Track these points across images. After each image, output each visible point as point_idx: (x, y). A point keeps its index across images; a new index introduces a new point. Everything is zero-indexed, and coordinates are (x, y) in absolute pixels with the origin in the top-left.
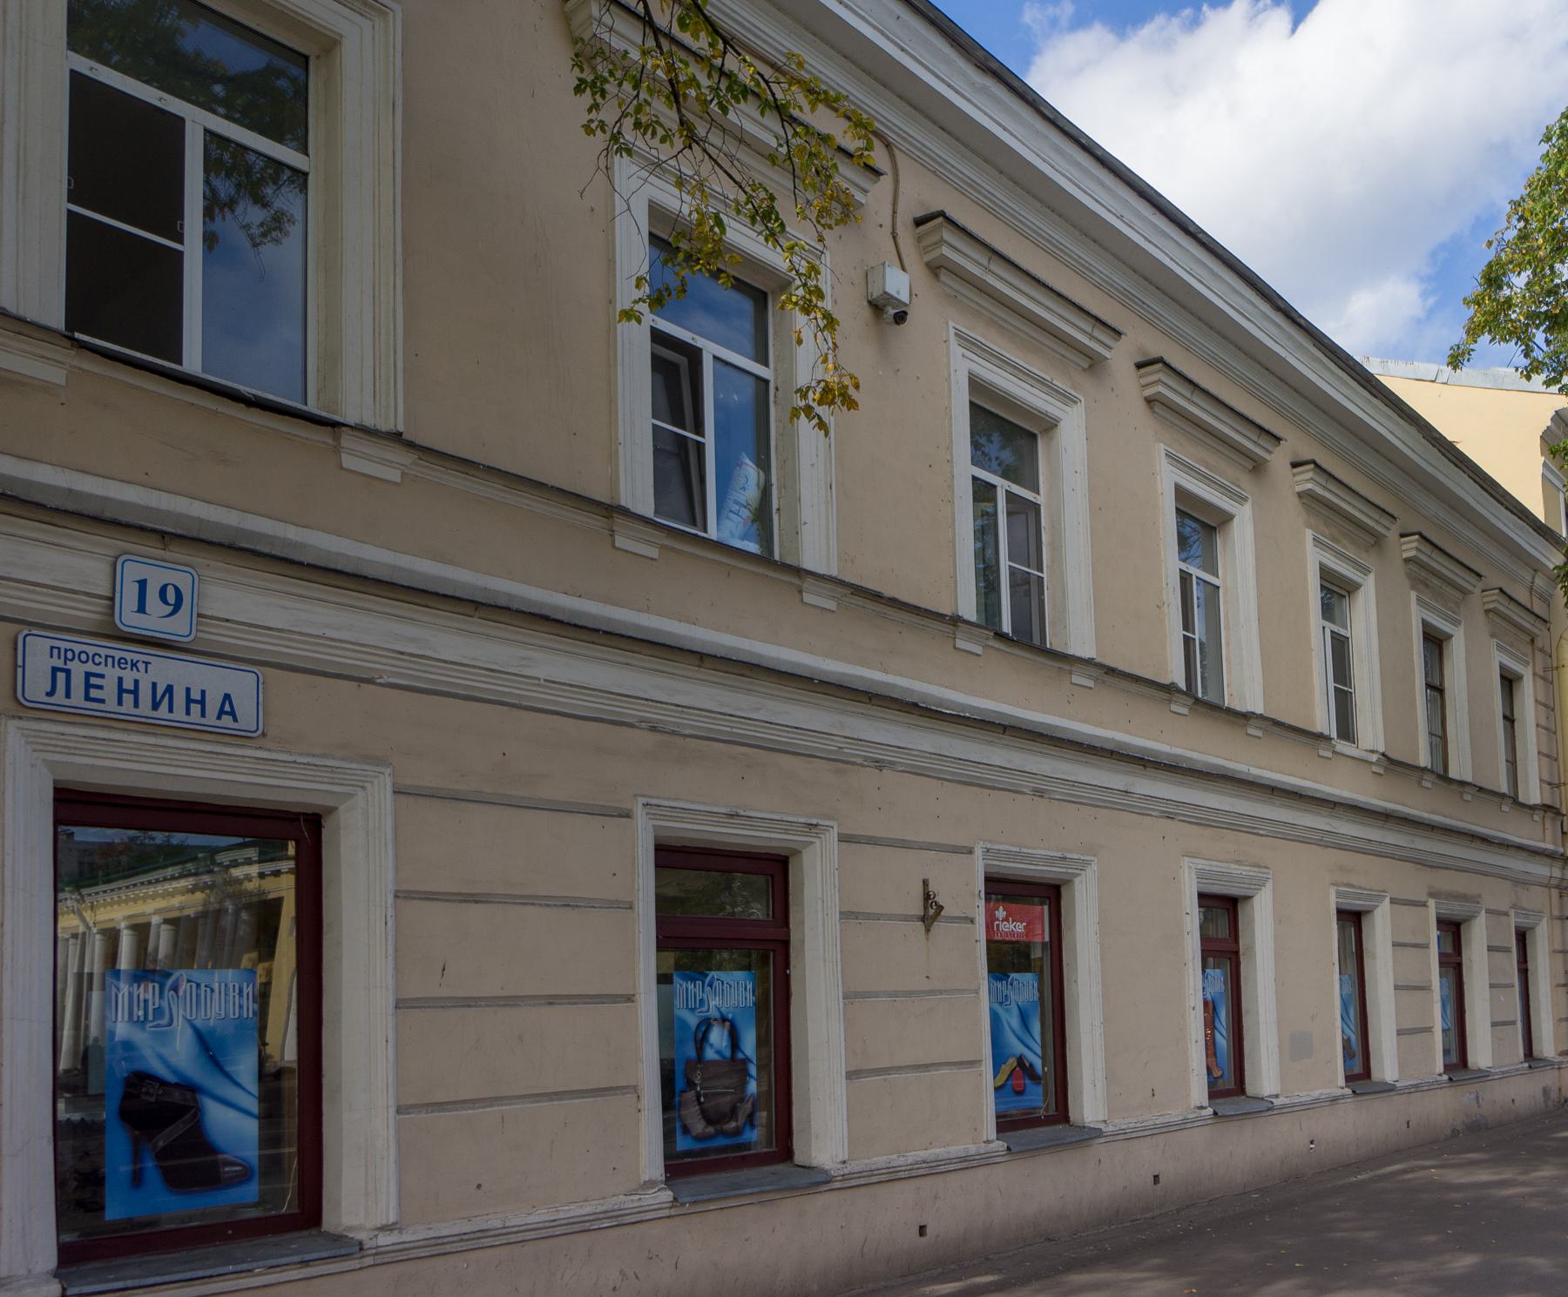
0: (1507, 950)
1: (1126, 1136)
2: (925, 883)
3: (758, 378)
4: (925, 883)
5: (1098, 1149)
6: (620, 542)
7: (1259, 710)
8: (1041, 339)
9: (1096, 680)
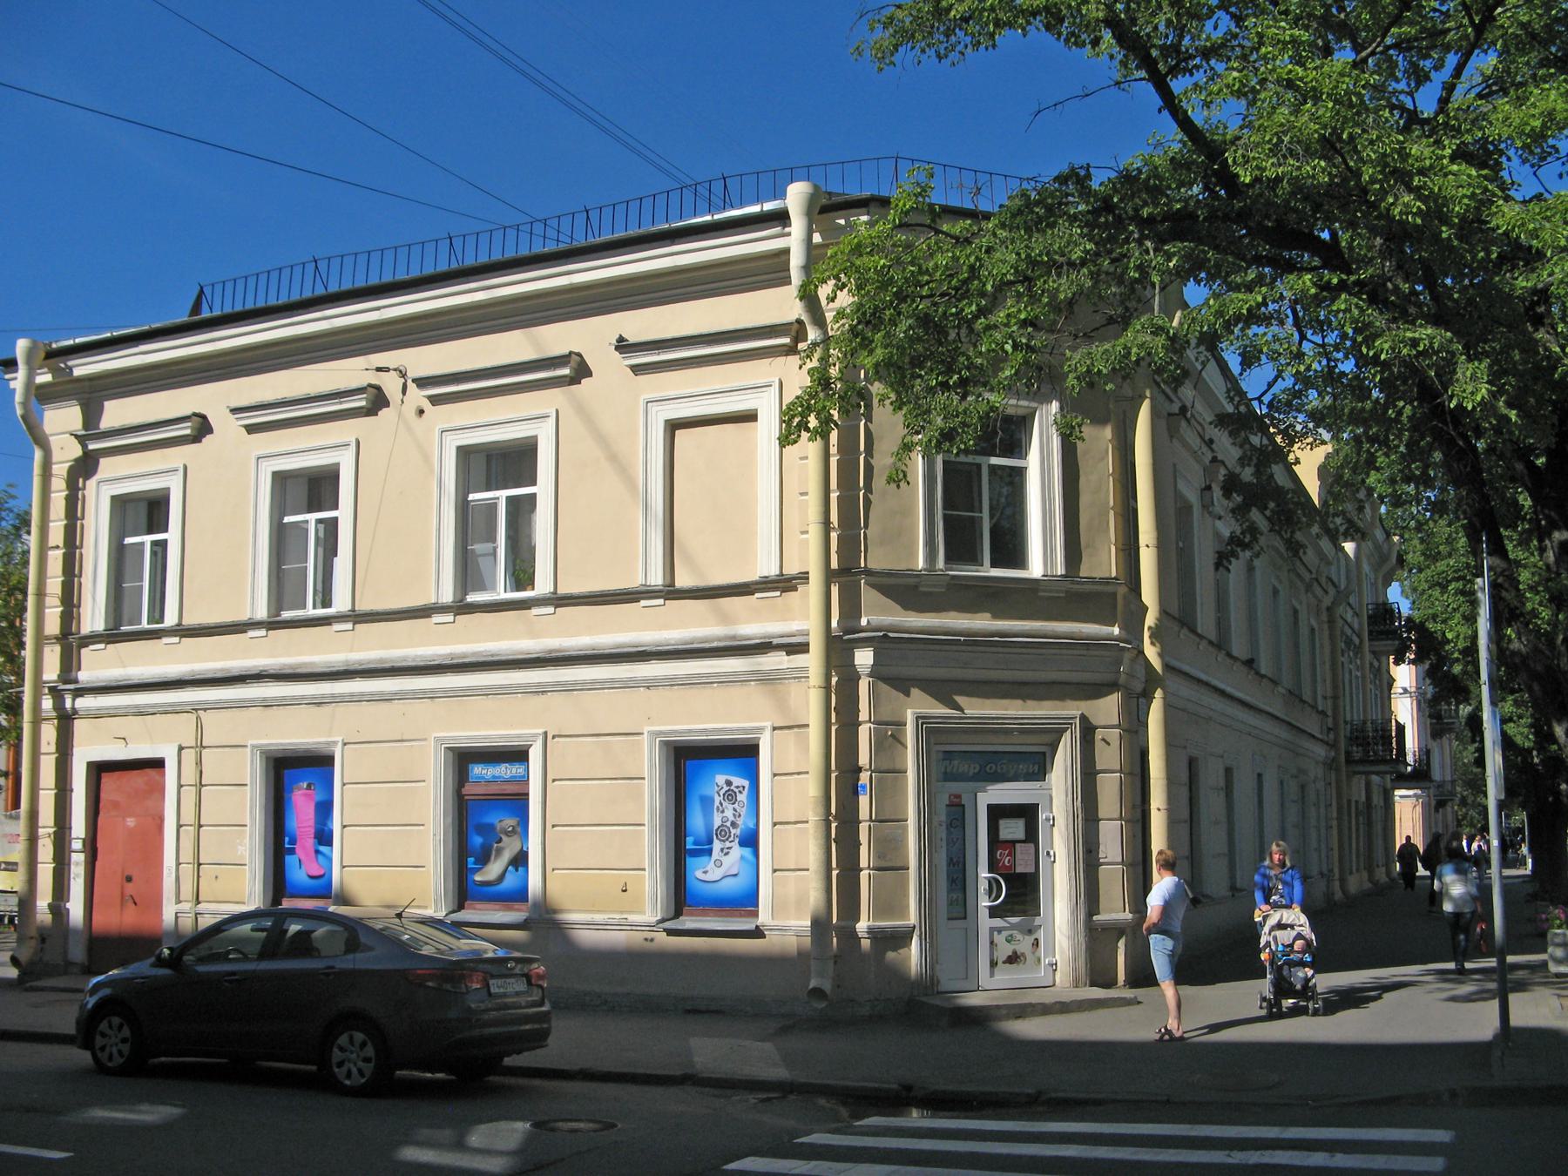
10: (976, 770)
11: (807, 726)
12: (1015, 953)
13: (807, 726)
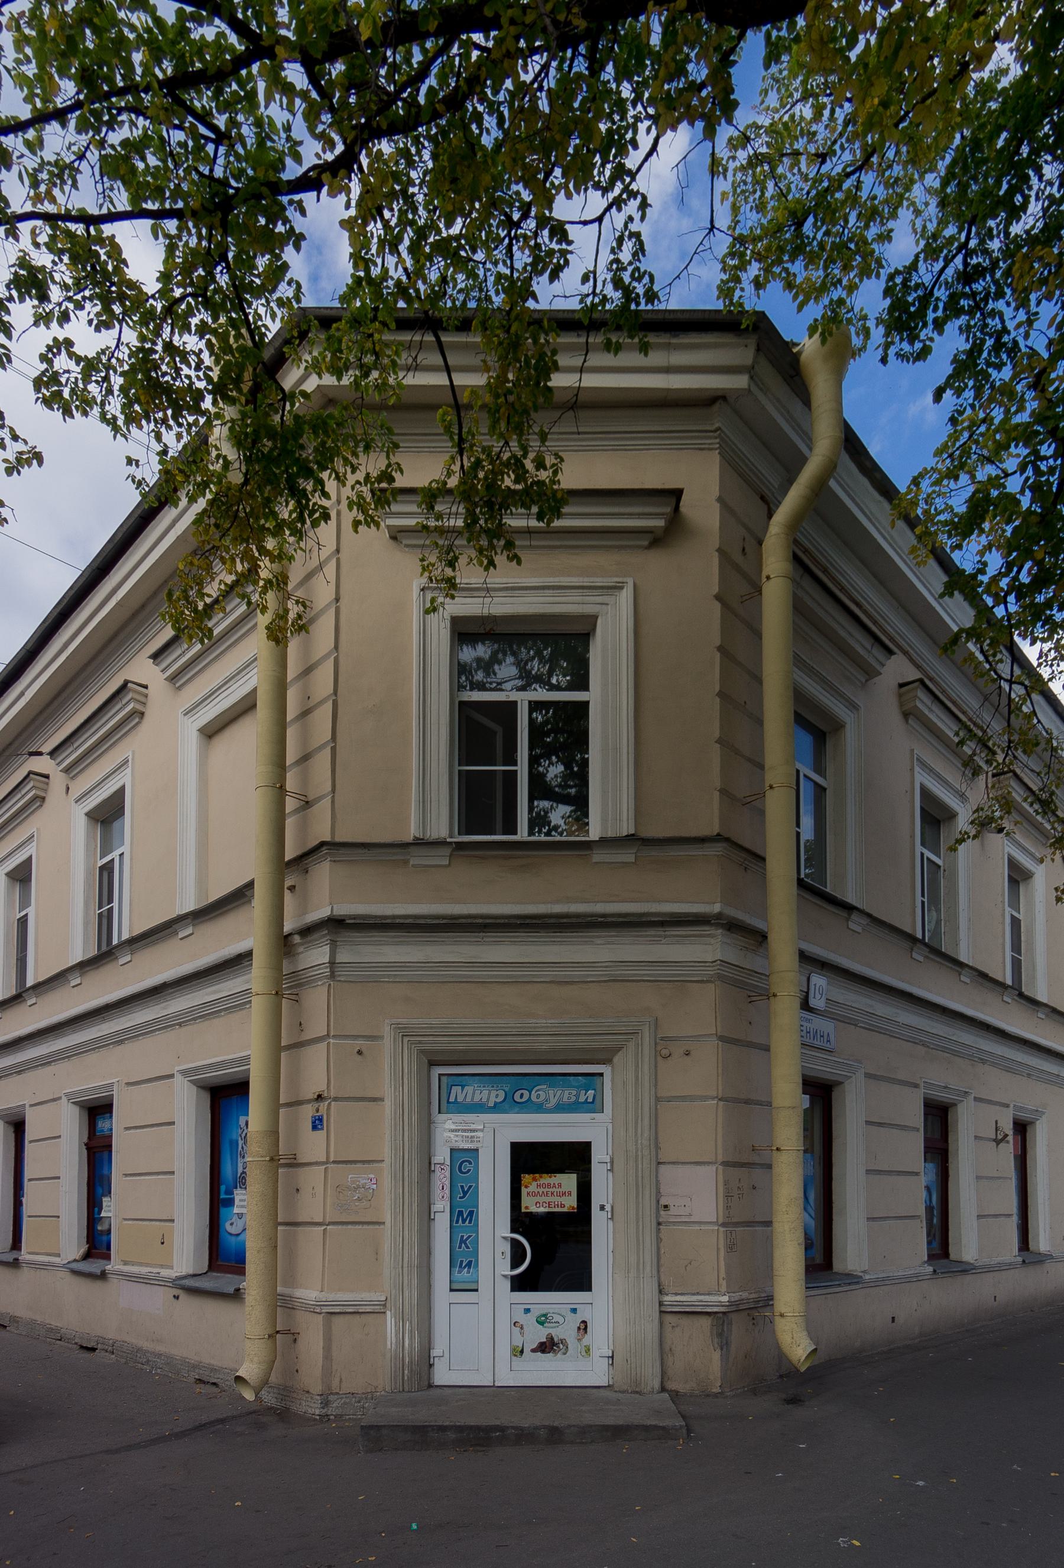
0: (918, 1130)
1: (990, 1269)
2: (996, 1122)
3: (816, 784)
4: (996, 1122)
5: (1048, 1266)
6: (915, 955)
7: (1045, 1001)
8: (920, 730)
9: (1047, 1016)
10: (499, 1100)
11: (382, 1100)
12: (551, 1339)
13: (382, 1100)
